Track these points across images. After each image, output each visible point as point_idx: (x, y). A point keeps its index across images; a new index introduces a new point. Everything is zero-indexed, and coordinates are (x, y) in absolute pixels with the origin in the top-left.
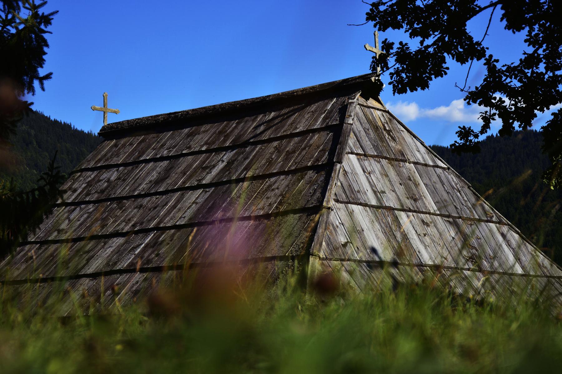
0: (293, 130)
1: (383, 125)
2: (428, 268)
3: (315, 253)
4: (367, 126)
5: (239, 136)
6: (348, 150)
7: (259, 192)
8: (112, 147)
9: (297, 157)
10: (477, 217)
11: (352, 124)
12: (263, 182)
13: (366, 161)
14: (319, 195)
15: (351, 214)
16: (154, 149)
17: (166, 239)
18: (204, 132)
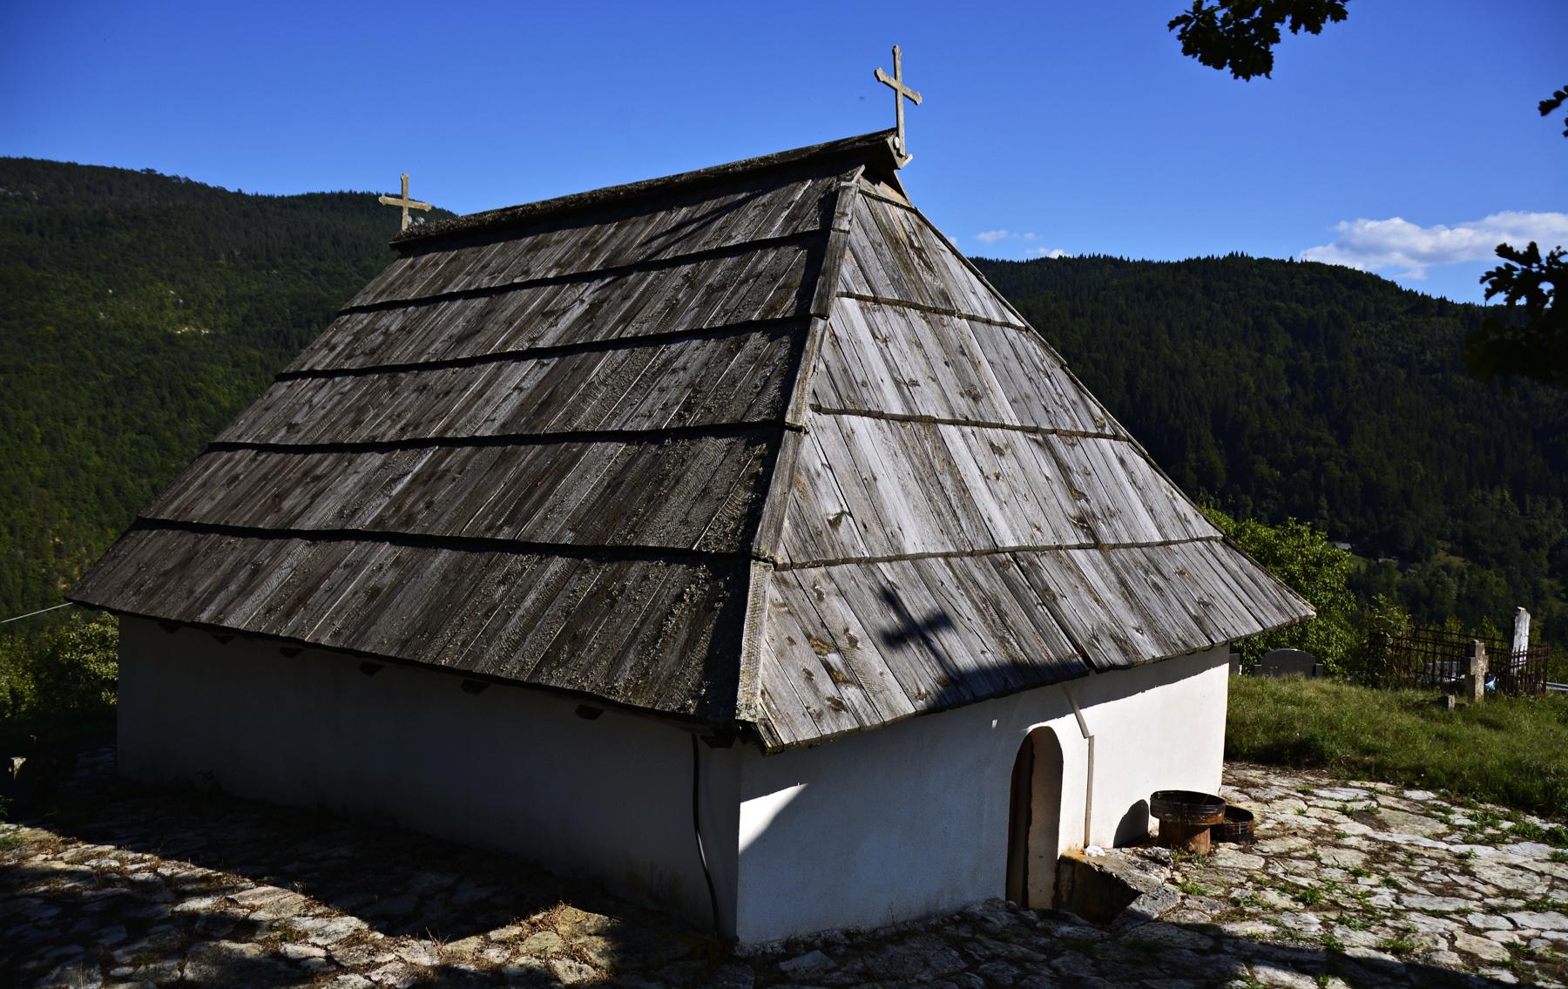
0: (723, 242)
1: (909, 237)
2: (1007, 554)
3: (764, 553)
4: (878, 237)
5: (618, 253)
6: (841, 288)
7: (644, 375)
8: (406, 269)
9: (729, 299)
10: (1082, 429)
11: (849, 232)
12: (655, 352)
13: (877, 314)
14: (776, 393)
15: (848, 438)
16: (469, 274)
17: (452, 466)
18: (557, 242)
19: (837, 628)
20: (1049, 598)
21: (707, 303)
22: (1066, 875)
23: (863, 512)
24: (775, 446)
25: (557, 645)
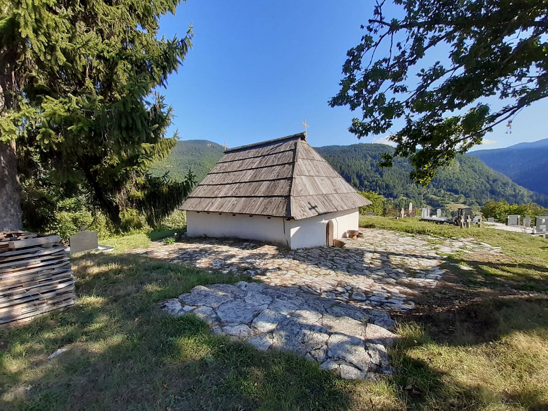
15: (302, 179)
19: (303, 205)
20: (330, 201)
21: (278, 160)
22: (335, 242)
23: (304, 189)
25: (264, 209)
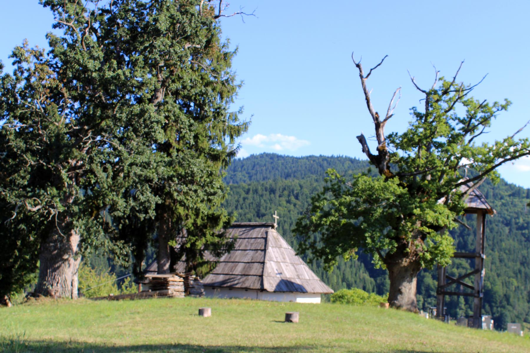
15: (271, 264)
24: (264, 264)
